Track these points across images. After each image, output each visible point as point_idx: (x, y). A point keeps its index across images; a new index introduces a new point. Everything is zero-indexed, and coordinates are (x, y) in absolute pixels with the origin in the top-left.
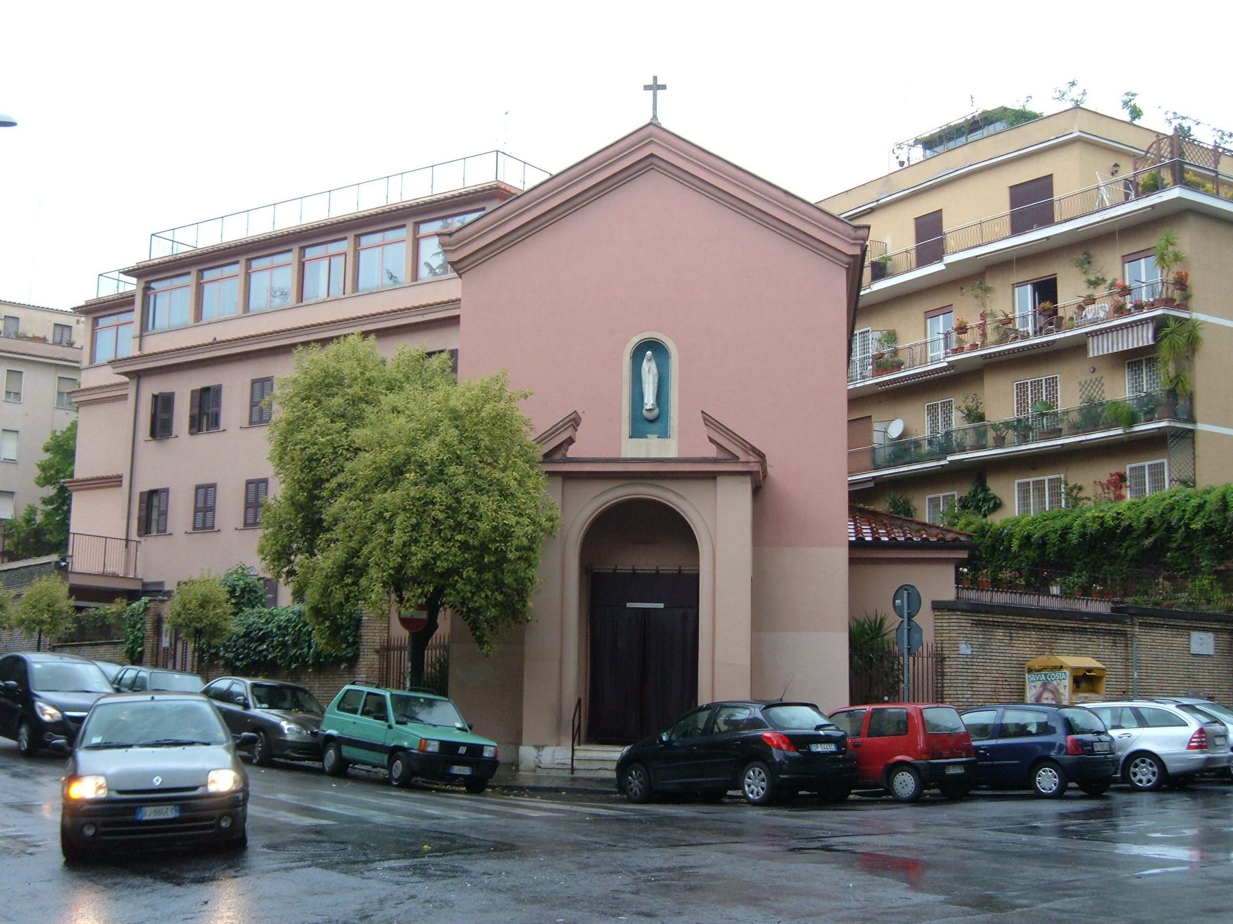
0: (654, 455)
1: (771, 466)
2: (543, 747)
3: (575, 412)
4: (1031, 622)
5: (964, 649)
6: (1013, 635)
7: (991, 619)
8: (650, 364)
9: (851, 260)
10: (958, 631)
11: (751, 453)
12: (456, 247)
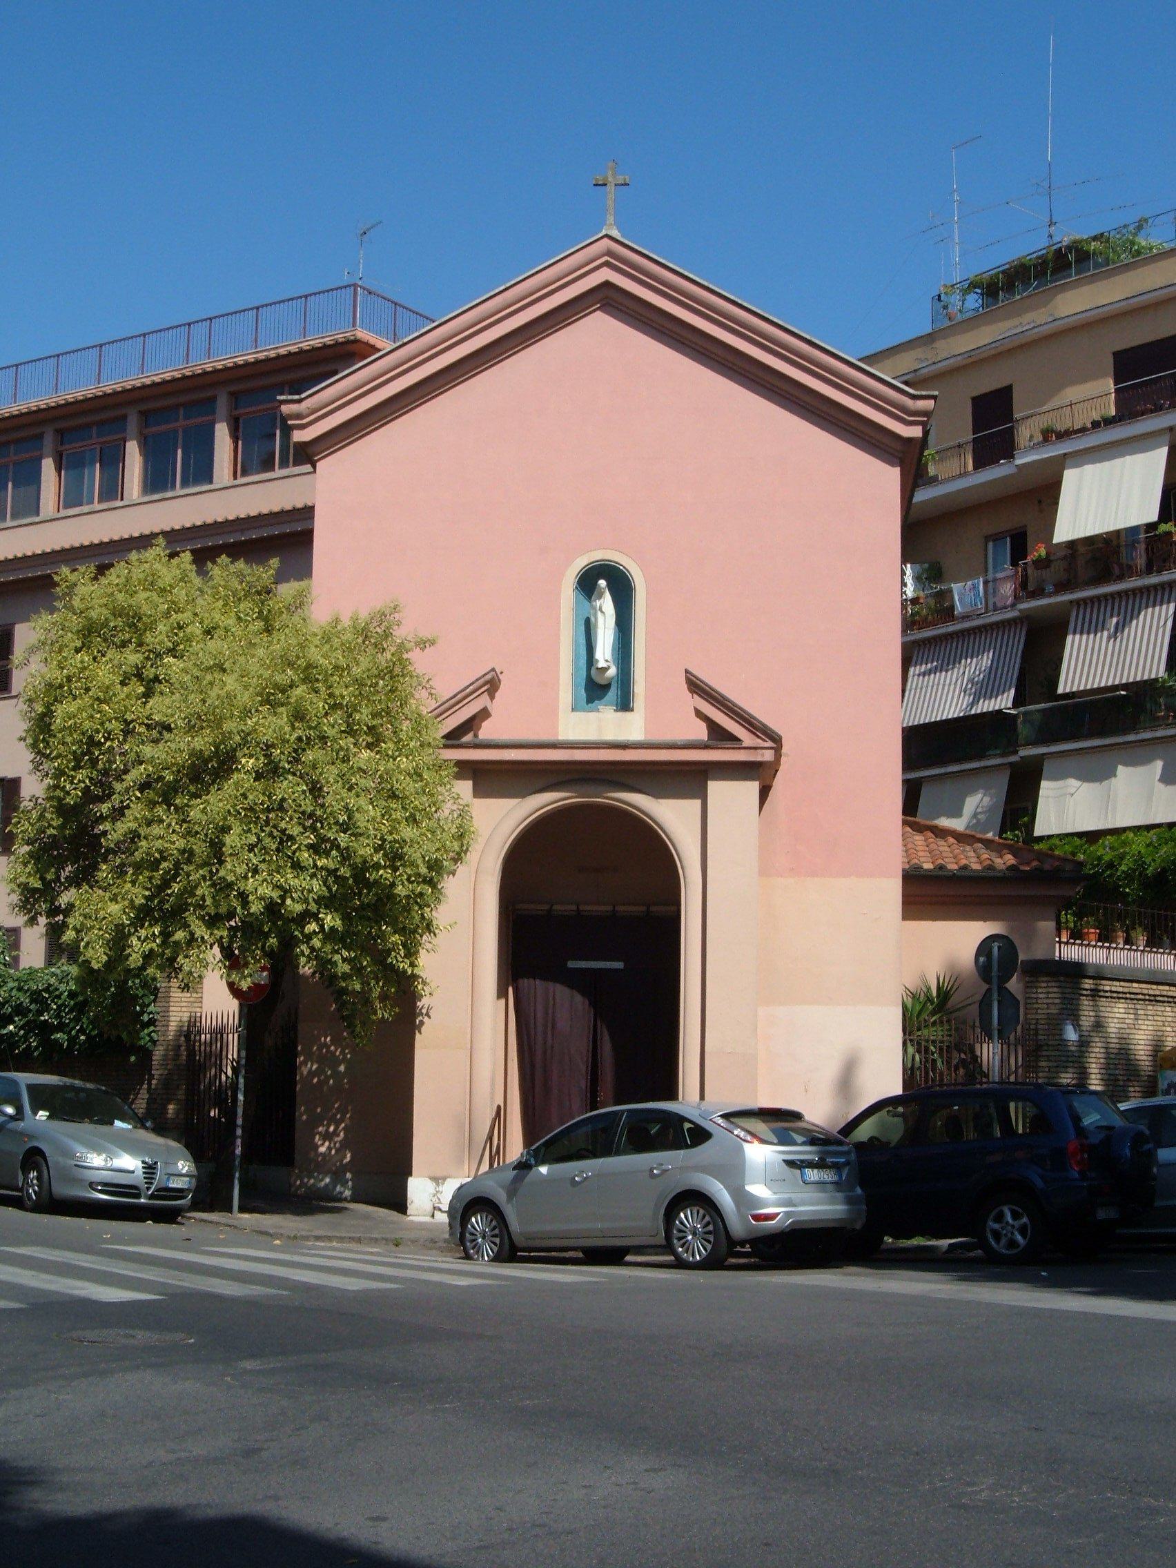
0: (610, 736)
2: (444, 1179)
3: (493, 670)
4: (1165, 993)
6: (1139, 1012)
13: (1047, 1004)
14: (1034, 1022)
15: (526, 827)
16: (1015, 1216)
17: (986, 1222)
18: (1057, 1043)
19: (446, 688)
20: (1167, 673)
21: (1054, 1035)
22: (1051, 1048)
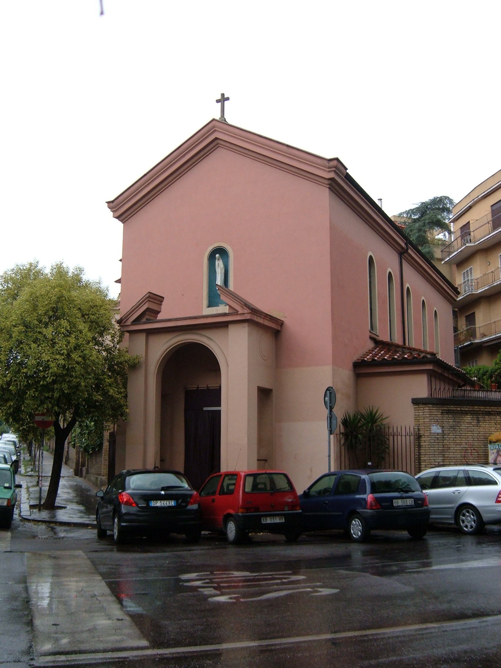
5: (436, 429)
7: (459, 409)
8: (219, 262)
9: (329, 182)
10: (430, 418)
11: (245, 307)
12: (117, 208)
16: (468, 512)
17: (459, 516)
18: (428, 434)
22: (426, 437)
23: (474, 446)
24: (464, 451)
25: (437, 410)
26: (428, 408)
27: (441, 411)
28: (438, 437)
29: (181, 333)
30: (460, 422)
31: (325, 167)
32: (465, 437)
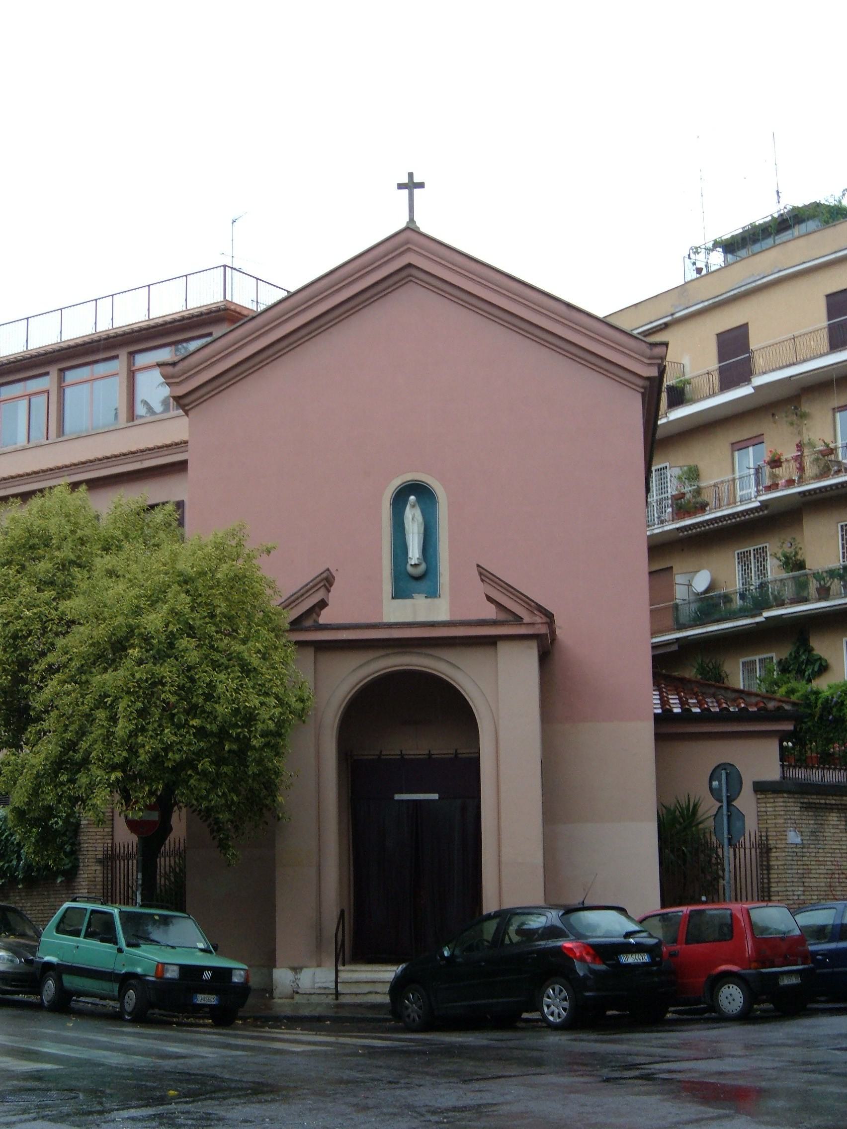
1: (560, 628)
2: (301, 969)
3: (328, 570)
5: (794, 837)
7: (823, 801)
9: (647, 383)
10: (785, 817)
13: (775, 815)
14: (765, 830)
15: (362, 687)
18: (783, 846)
19: (289, 585)
20: (694, 607)
21: (781, 840)
22: (779, 850)
23: (842, 867)
24: (830, 876)
25: (794, 802)
26: (782, 800)
27: (799, 805)
28: (797, 850)
29: (390, 651)
30: (824, 824)
31: (643, 356)
32: (831, 851)
